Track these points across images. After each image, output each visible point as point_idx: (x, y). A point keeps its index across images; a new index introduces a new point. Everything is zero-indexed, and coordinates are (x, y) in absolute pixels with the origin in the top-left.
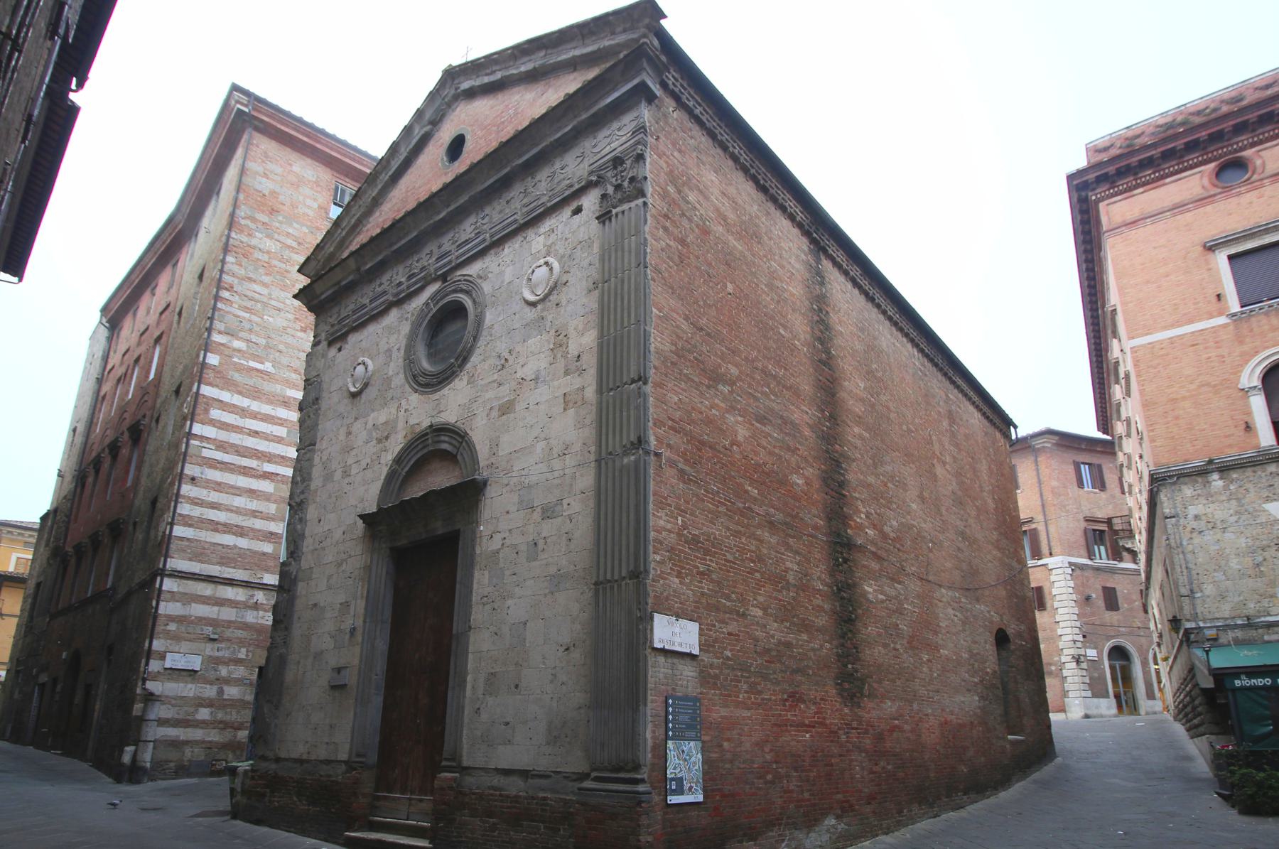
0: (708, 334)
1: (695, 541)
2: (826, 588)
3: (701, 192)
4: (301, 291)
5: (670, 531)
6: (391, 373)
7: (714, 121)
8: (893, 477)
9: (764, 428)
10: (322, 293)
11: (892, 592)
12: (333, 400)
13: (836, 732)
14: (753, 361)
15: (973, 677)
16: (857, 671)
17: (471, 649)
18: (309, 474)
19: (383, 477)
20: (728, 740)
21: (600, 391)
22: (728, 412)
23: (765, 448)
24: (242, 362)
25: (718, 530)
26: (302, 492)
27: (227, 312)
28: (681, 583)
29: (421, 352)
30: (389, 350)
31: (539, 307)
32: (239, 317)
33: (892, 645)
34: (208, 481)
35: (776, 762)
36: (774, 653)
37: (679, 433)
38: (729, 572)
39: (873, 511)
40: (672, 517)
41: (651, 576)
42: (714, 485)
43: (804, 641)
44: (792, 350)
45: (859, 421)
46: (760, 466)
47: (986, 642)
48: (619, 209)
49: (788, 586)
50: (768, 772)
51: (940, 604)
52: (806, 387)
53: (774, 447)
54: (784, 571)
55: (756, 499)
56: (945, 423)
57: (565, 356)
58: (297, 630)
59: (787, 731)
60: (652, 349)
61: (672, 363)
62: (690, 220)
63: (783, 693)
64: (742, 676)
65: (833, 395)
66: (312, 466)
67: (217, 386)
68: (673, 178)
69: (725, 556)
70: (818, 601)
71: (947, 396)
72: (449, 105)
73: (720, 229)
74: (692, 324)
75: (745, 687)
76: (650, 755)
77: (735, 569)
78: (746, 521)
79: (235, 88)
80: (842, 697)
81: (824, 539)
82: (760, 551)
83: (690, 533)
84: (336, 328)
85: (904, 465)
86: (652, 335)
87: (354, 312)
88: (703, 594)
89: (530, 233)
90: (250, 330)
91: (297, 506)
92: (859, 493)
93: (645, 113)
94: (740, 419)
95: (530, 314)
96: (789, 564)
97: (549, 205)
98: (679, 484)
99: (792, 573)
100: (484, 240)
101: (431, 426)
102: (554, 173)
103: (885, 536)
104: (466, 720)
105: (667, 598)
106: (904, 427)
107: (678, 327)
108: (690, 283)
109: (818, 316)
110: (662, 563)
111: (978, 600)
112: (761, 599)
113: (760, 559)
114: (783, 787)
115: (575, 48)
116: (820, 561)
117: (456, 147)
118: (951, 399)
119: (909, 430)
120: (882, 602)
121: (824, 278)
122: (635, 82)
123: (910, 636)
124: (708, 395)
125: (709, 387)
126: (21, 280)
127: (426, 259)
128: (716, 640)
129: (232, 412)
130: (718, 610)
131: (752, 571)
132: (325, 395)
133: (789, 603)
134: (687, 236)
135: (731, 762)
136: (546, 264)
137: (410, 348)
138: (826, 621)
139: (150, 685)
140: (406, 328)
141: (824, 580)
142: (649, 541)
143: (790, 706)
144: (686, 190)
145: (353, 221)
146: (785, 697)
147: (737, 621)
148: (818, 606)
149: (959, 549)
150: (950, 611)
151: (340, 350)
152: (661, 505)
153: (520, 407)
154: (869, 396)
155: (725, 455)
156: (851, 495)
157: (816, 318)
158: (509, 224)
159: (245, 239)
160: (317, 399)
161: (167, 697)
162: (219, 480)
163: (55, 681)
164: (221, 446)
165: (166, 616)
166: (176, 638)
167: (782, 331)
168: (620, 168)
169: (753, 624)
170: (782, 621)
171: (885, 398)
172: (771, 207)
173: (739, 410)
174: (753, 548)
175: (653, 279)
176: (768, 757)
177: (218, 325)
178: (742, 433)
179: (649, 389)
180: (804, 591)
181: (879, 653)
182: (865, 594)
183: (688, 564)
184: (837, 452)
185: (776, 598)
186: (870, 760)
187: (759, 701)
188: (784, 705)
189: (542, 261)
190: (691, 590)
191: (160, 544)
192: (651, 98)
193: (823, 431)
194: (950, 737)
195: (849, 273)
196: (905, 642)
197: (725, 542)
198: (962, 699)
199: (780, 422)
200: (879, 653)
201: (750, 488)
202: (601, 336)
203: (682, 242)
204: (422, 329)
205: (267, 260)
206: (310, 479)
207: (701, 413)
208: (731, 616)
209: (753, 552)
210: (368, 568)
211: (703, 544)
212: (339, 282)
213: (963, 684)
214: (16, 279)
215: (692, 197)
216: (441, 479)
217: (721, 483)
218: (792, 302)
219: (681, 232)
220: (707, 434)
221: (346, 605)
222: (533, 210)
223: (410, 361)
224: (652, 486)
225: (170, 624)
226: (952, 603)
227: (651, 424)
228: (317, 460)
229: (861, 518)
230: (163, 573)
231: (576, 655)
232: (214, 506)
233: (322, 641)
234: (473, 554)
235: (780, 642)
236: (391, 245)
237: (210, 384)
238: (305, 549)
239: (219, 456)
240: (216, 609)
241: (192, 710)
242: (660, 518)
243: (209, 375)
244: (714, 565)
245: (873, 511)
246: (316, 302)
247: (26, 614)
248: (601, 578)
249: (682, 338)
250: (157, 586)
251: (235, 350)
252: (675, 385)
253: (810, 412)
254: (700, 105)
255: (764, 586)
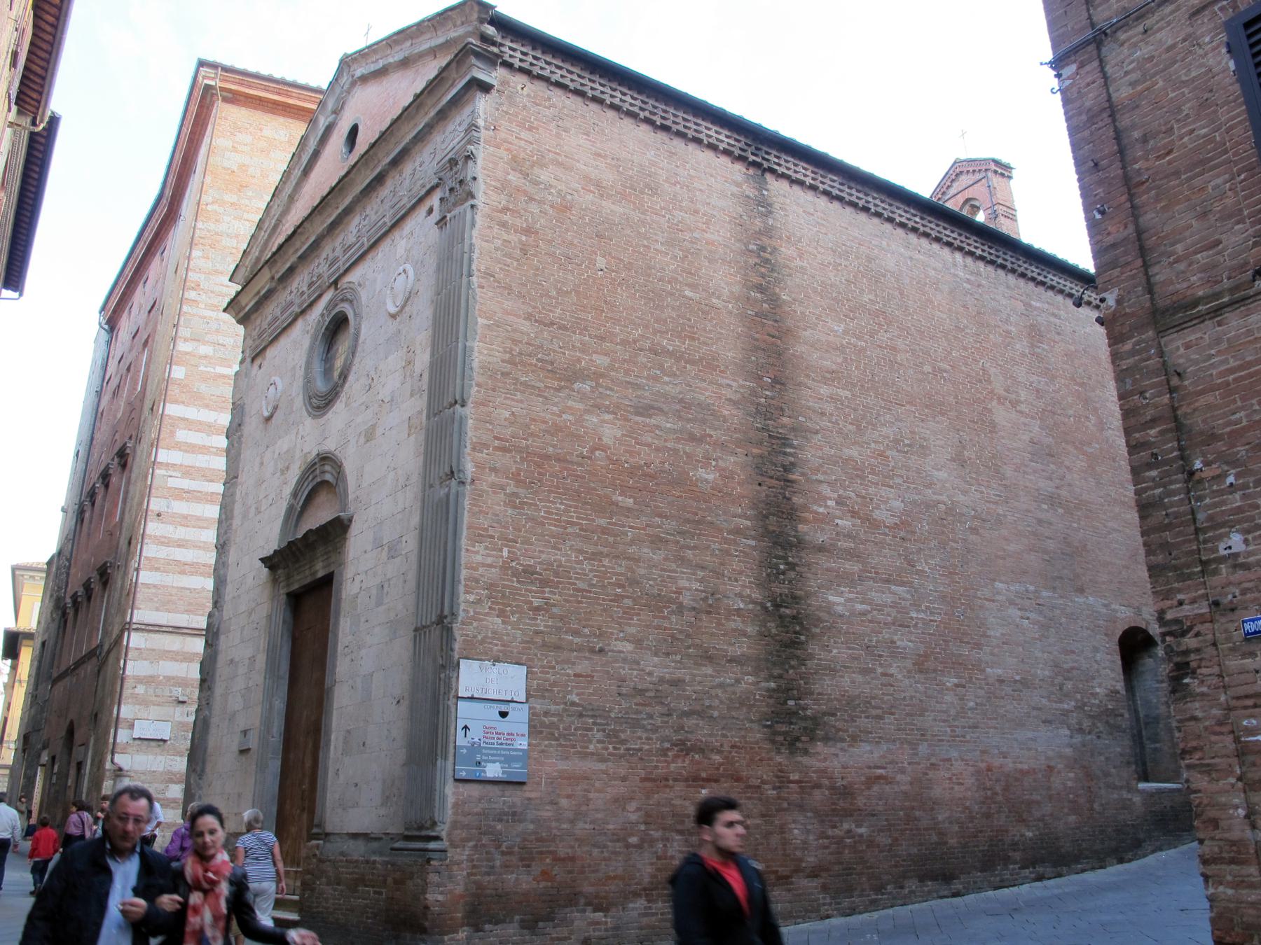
0: (564, 328)
1: (529, 572)
2: (750, 606)
3: (560, 164)
4: (229, 304)
5: (490, 566)
6: (294, 394)
7: (583, 78)
8: (896, 441)
9: (648, 420)
10: (247, 305)
11: (888, 599)
12: (252, 425)
13: (759, 787)
14: (635, 342)
15: (1061, 702)
16: (804, 709)
17: (335, 706)
18: (232, 511)
19: (283, 514)
20: (569, 797)
21: (428, 417)
22: (587, 412)
23: (649, 445)
24: (208, 369)
25: (565, 556)
26: (226, 533)
27: (194, 315)
28: (504, 623)
29: (317, 368)
30: (294, 368)
31: (398, 319)
32: (205, 318)
33: (879, 670)
34: (174, 515)
35: (646, 823)
36: (652, 694)
37: (509, 451)
38: (580, 602)
39: (853, 495)
40: (494, 550)
41: (460, 619)
42: (561, 503)
43: (706, 676)
44: (707, 313)
45: (831, 377)
46: (640, 467)
47: (1096, 650)
48: (453, 213)
49: (681, 609)
50: (632, 835)
51: (992, 605)
52: (730, 352)
53: (666, 441)
54: (675, 593)
55: (629, 510)
56: (1021, 346)
57: (412, 377)
58: (219, 690)
59: (666, 786)
60: (475, 364)
61: (502, 374)
62: (539, 202)
63: (662, 742)
64: (594, 724)
65: (780, 355)
66: (234, 502)
67: (183, 403)
68: (516, 163)
69: (575, 584)
70: (736, 623)
71: (1027, 305)
72: (348, 92)
73: (590, 197)
74: (536, 321)
75: (599, 736)
76: (450, 812)
77: (590, 598)
78: (611, 539)
79: (202, 64)
80: (773, 742)
81: (753, 543)
82: (633, 572)
83: (522, 565)
84: (257, 343)
85: (923, 421)
86: (476, 349)
87: (270, 325)
88: (537, 633)
89: (396, 234)
90: (217, 331)
91: (222, 547)
92: (825, 473)
93: (482, 105)
94: (608, 417)
95: (392, 326)
96: (683, 583)
97: (408, 206)
98: (506, 511)
99: (688, 593)
100: (363, 244)
101: (318, 455)
102: (415, 170)
103: (875, 525)
104: (329, 783)
105: (482, 642)
106: (928, 368)
107: (515, 330)
108: (536, 275)
109: (759, 256)
110: (479, 601)
111: (1081, 591)
112: (633, 630)
113: (634, 582)
114: (656, 853)
115: (431, 39)
116: (741, 573)
117: (354, 131)
118: (1036, 308)
119: (937, 371)
120: (864, 614)
121: (770, 205)
122: (468, 78)
123: (920, 655)
124: (556, 400)
125: (558, 390)
126: (21, 295)
127: (320, 267)
128: (555, 684)
129: (199, 431)
130: (558, 648)
131: (618, 599)
132: (247, 419)
133: (681, 632)
134: (535, 223)
135: (572, 822)
136: (404, 271)
137: (308, 364)
138: (749, 648)
139: (119, 759)
140: (306, 343)
141: (749, 596)
142: (459, 582)
143: (676, 756)
144: (536, 170)
145: (273, 221)
146: (667, 745)
147: (589, 659)
148: (735, 630)
149: (1040, 521)
150: (1014, 612)
151: (260, 367)
152: (478, 537)
153: (379, 431)
154: (853, 340)
155: (581, 465)
156: (808, 480)
157: (752, 261)
158: (381, 228)
159: (212, 227)
160: (240, 425)
161: (136, 772)
162: (185, 512)
163: (53, 758)
164: (188, 472)
165: (134, 677)
166: (144, 702)
167: (688, 293)
168: (455, 169)
169: (616, 661)
170: (668, 654)
171: (888, 335)
172: (678, 143)
173: (608, 407)
174: (622, 570)
175: (482, 287)
176: (633, 817)
177: (184, 332)
178: (610, 432)
179: (469, 410)
180: (709, 613)
181: (853, 682)
182: (829, 608)
183: (515, 600)
184: (783, 426)
185: (658, 627)
186: (823, 821)
187: (622, 751)
188: (666, 755)
189: (401, 269)
190: (520, 629)
191: (128, 594)
192: (486, 88)
193: (758, 404)
194: (998, 789)
195: (818, 188)
196: (909, 664)
197: (575, 568)
198: (1030, 734)
199: (678, 407)
200: (853, 682)
201: (620, 498)
202: (432, 355)
203: (528, 231)
204: (318, 343)
205: (235, 245)
206: (232, 518)
207: (545, 422)
208: (581, 655)
209: (622, 574)
210: (269, 617)
211: (541, 574)
212: (259, 292)
213: (1035, 713)
214: (16, 295)
215: (544, 175)
216: (320, 516)
217: (572, 500)
218: (710, 251)
219: (526, 220)
220: (554, 446)
221: (253, 659)
222: (397, 212)
223: (308, 381)
224: (466, 518)
225: (138, 686)
226: (1018, 601)
227: (468, 450)
228: (238, 493)
229: (827, 507)
230: (126, 627)
231: (405, 704)
232: (181, 544)
233: (236, 703)
234: (339, 601)
235: (662, 680)
236: (297, 250)
237: (176, 402)
238: (227, 598)
239: (186, 484)
240: (185, 665)
241: (162, 786)
242: (477, 553)
243: (174, 391)
244: (557, 597)
245: (853, 495)
246: (242, 314)
247: (33, 680)
248: (419, 625)
249: (521, 342)
250: (125, 643)
251: (201, 357)
252: (506, 398)
253: (734, 384)
254: (560, 68)
255: (639, 614)
